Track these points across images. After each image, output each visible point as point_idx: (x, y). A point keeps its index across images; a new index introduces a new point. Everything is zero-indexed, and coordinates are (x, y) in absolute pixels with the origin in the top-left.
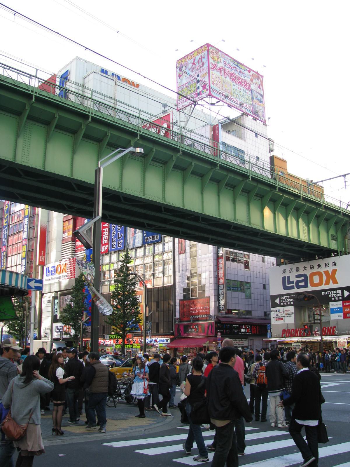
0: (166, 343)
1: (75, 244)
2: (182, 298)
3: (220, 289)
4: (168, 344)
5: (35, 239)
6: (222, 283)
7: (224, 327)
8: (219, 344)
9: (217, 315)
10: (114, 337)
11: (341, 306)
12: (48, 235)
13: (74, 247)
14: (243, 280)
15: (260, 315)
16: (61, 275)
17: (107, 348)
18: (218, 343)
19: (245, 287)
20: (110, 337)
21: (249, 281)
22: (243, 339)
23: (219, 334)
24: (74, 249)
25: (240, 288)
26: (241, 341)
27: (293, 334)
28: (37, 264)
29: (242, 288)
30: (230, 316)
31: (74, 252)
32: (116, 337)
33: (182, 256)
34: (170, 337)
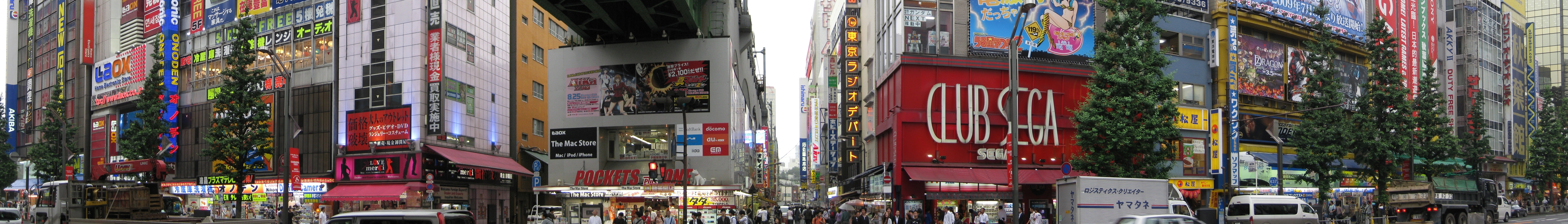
0: (318, 191)
1: (143, 23)
2: (352, 108)
3: (432, 91)
4: (322, 193)
5: (76, 22)
6: (438, 80)
7: (435, 165)
8: (430, 196)
9: (424, 141)
10: (218, 181)
11: (701, 132)
12: (97, 12)
13: (142, 29)
14: (464, 81)
15: (485, 148)
16: (120, 78)
17: (202, 200)
18: (428, 194)
19: (467, 95)
20: (209, 180)
21: (473, 84)
22: (461, 188)
23: (430, 177)
24: (142, 32)
25: (460, 94)
26: (458, 192)
27: (600, 181)
28: (81, 61)
29: (462, 94)
30: (444, 144)
31: (142, 36)
32: (222, 180)
33: (354, 27)
34: (328, 181)
